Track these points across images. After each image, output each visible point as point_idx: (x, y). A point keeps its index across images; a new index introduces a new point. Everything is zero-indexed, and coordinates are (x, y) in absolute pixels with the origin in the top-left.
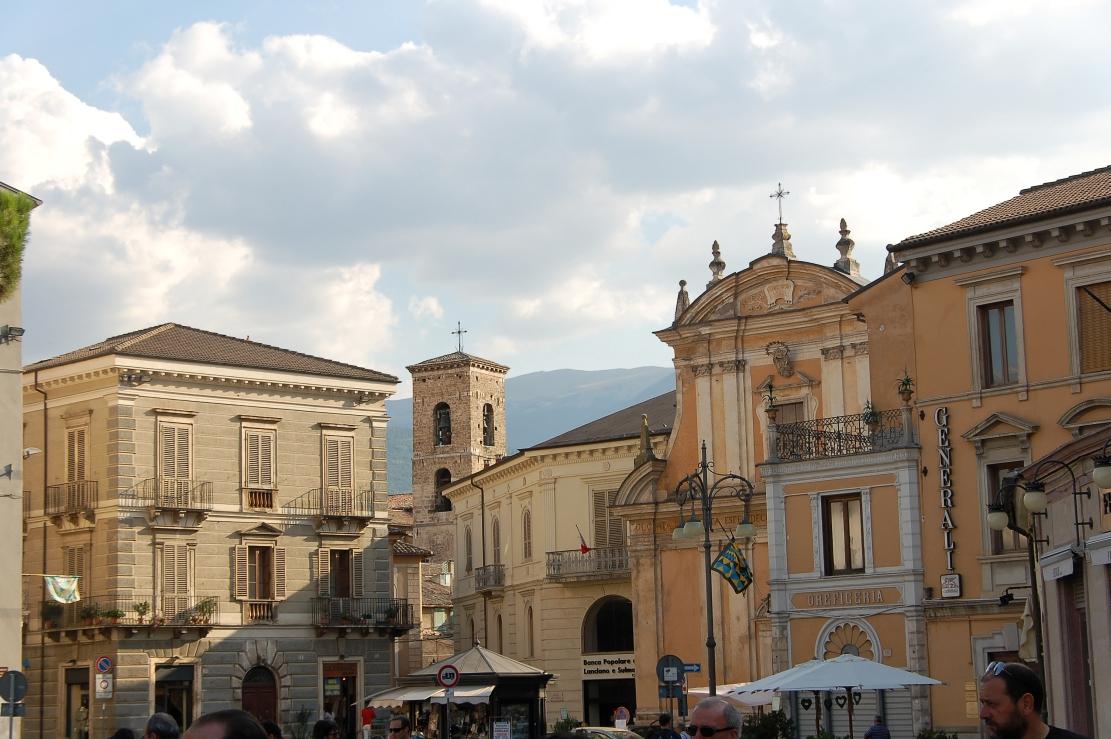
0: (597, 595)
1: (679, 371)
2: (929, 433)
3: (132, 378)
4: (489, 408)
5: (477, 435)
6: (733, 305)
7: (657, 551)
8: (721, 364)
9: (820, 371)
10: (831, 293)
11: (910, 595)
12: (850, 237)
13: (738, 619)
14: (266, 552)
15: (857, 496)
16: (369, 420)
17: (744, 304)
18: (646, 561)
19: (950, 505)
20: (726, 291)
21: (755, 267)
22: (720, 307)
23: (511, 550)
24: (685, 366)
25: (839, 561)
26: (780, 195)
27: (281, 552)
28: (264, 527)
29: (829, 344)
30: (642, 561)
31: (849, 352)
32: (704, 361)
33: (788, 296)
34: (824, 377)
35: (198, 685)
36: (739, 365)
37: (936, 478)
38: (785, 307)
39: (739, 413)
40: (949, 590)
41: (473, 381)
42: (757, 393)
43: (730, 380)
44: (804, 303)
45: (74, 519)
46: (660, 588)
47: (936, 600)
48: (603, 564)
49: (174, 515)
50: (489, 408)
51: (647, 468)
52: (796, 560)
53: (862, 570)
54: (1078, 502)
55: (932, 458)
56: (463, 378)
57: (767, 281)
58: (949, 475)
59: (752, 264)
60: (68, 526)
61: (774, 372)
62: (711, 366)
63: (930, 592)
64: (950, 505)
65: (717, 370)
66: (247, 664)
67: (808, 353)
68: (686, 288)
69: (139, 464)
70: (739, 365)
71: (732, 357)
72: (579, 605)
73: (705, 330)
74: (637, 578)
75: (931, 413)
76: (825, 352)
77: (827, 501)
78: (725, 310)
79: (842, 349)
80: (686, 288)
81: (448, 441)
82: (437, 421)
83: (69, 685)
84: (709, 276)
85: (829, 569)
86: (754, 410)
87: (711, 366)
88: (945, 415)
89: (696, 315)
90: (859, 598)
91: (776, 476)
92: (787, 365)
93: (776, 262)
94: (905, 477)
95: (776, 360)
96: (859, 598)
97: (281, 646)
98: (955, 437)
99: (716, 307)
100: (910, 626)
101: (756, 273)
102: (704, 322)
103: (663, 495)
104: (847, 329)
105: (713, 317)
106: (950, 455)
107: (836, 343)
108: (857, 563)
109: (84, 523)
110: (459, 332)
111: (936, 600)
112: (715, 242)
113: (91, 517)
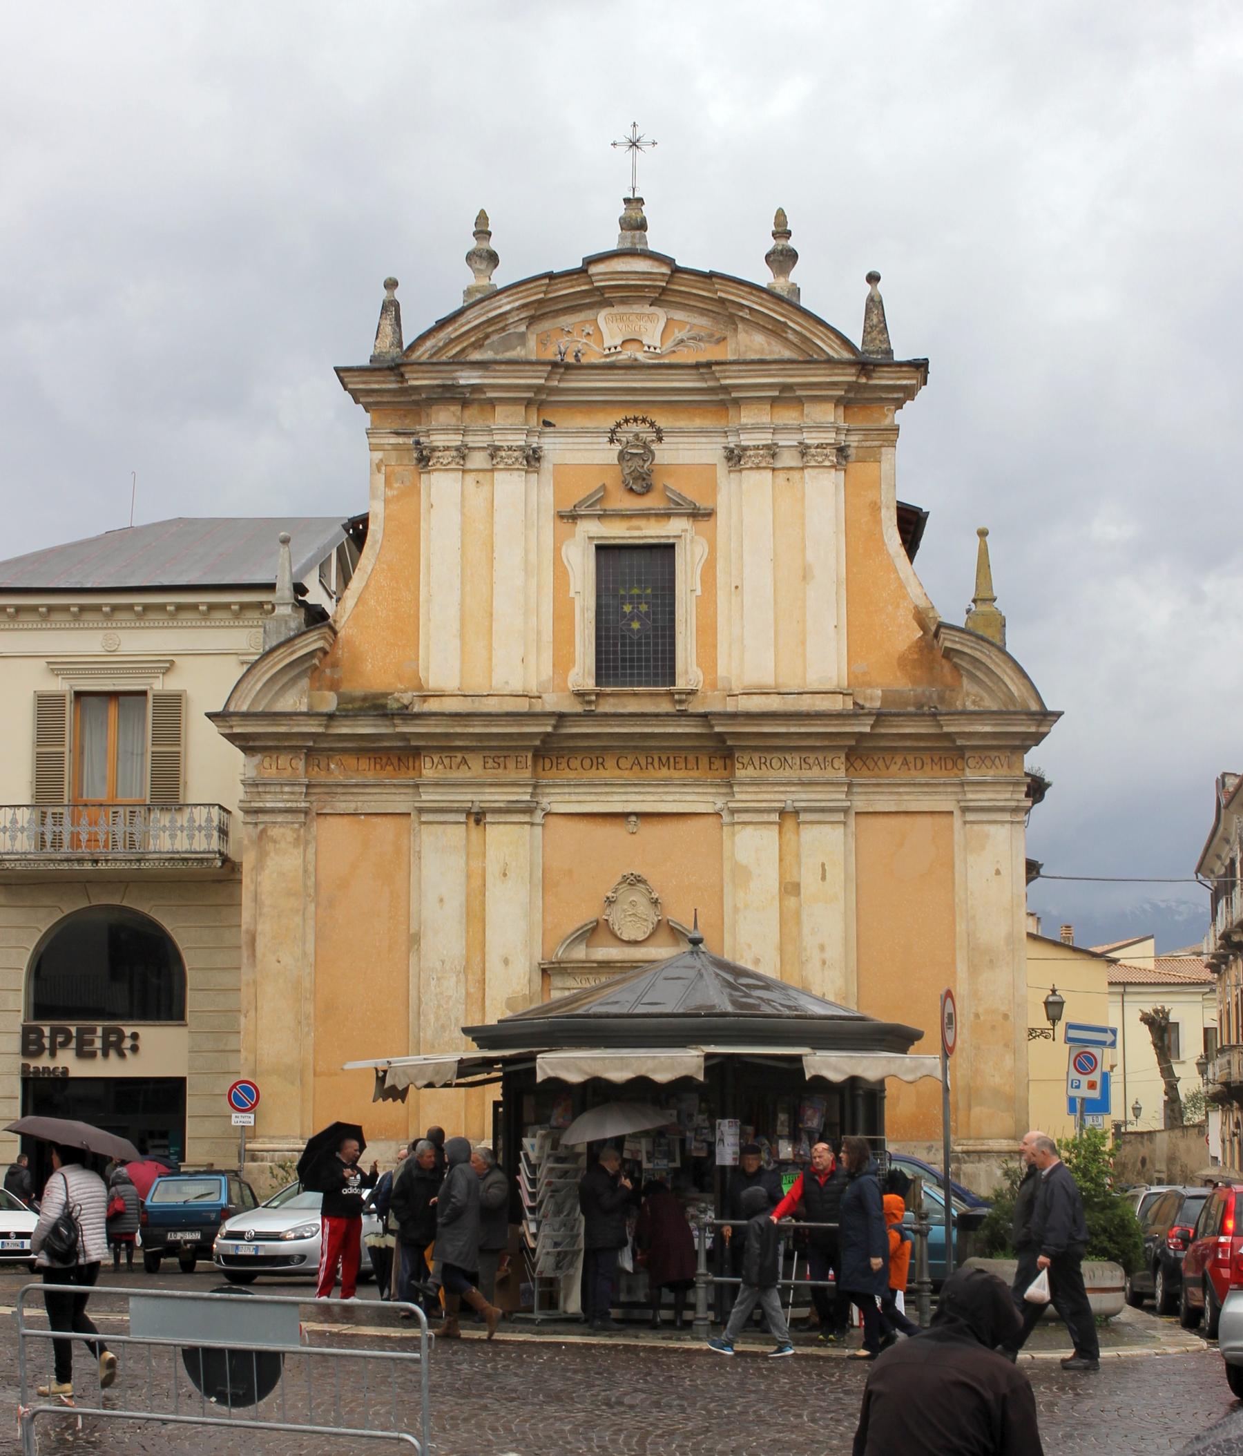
1: (379, 455)
8: (494, 452)
9: (713, 488)
12: (792, 243)
13: (506, 962)
20: (518, 309)
21: (593, 269)
22: (495, 338)
24: (396, 447)
26: (634, 144)
30: (274, 832)
34: (723, 503)
38: (641, 357)
39: (527, 552)
48: (49, 838)
54: (765, 817)
57: (609, 303)
59: (590, 261)
65: (478, 460)
68: (398, 294)
70: (533, 458)
71: (519, 440)
74: (259, 866)
76: (735, 457)
79: (772, 451)
80: (398, 294)
84: (467, 277)
86: (557, 551)
87: (462, 453)
89: (446, 345)
95: (622, 456)
99: (487, 336)
101: (574, 291)
105: (476, 356)
110: (634, 144)
112: (483, 212)
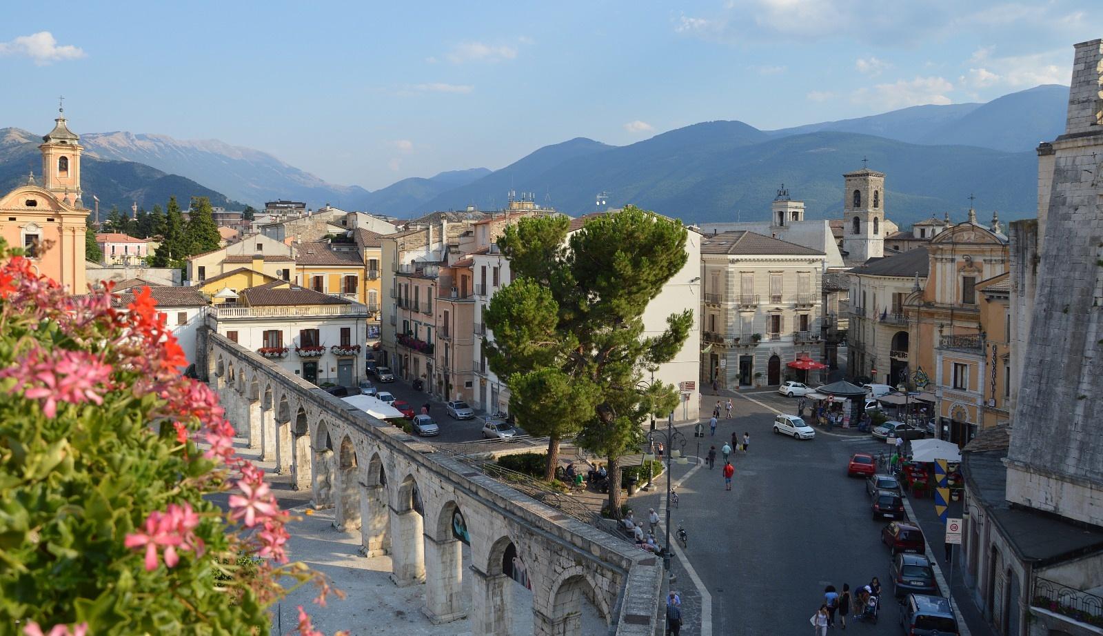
0: (898, 331)
2: (990, 351)
3: (733, 262)
4: (877, 192)
5: (871, 203)
6: (951, 238)
7: (919, 322)
10: (988, 239)
11: (980, 402)
14: (778, 317)
15: (966, 365)
16: (816, 268)
17: (956, 237)
18: (915, 326)
19: (994, 377)
23: (869, 307)
25: (959, 385)
27: (783, 317)
28: (777, 309)
29: (987, 258)
31: (993, 262)
32: (940, 257)
33: (972, 237)
34: (984, 269)
35: (754, 363)
36: (953, 260)
37: (991, 367)
40: (992, 404)
41: (870, 182)
42: (959, 271)
43: (949, 265)
44: (978, 241)
45: (714, 306)
46: (919, 335)
47: (987, 406)
49: (747, 304)
50: (877, 192)
51: (916, 294)
52: (945, 381)
53: (965, 389)
55: (990, 360)
56: (866, 181)
58: (994, 368)
60: (711, 307)
61: (966, 264)
62: (942, 259)
63: (985, 403)
64: (994, 377)
66: (770, 355)
67: (978, 259)
69: (736, 290)
70: (953, 260)
72: (891, 333)
73: (941, 247)
75: (991, 346)
77: (956, 365)
78: (948, 239)
79: (991, 260)
81: (858, 205)
82: (855, 197)
83: (712, 359)
85: (955, 387)
87: (942, 259)
88: (995, 347)
90: (964, 398)
91: (941, 354)
92: (970, 263)
93: (968, 225)
94: (981, 364)
95: (967, 261)
96: (964, 398)
97: (782, 348)
98: (998, 355)
100: (979, 412)
102: (942, 244)
103: (922, 303)
104: (994, 253)
106: (996, 361)
107: (989, 258)
108: (964, 387)
109: (717, 308)
111: (987, 406)
113: (719, 306)
